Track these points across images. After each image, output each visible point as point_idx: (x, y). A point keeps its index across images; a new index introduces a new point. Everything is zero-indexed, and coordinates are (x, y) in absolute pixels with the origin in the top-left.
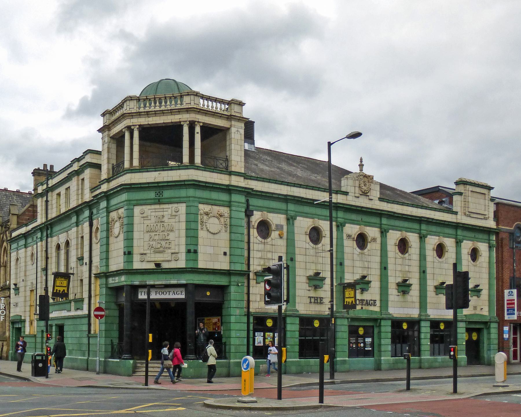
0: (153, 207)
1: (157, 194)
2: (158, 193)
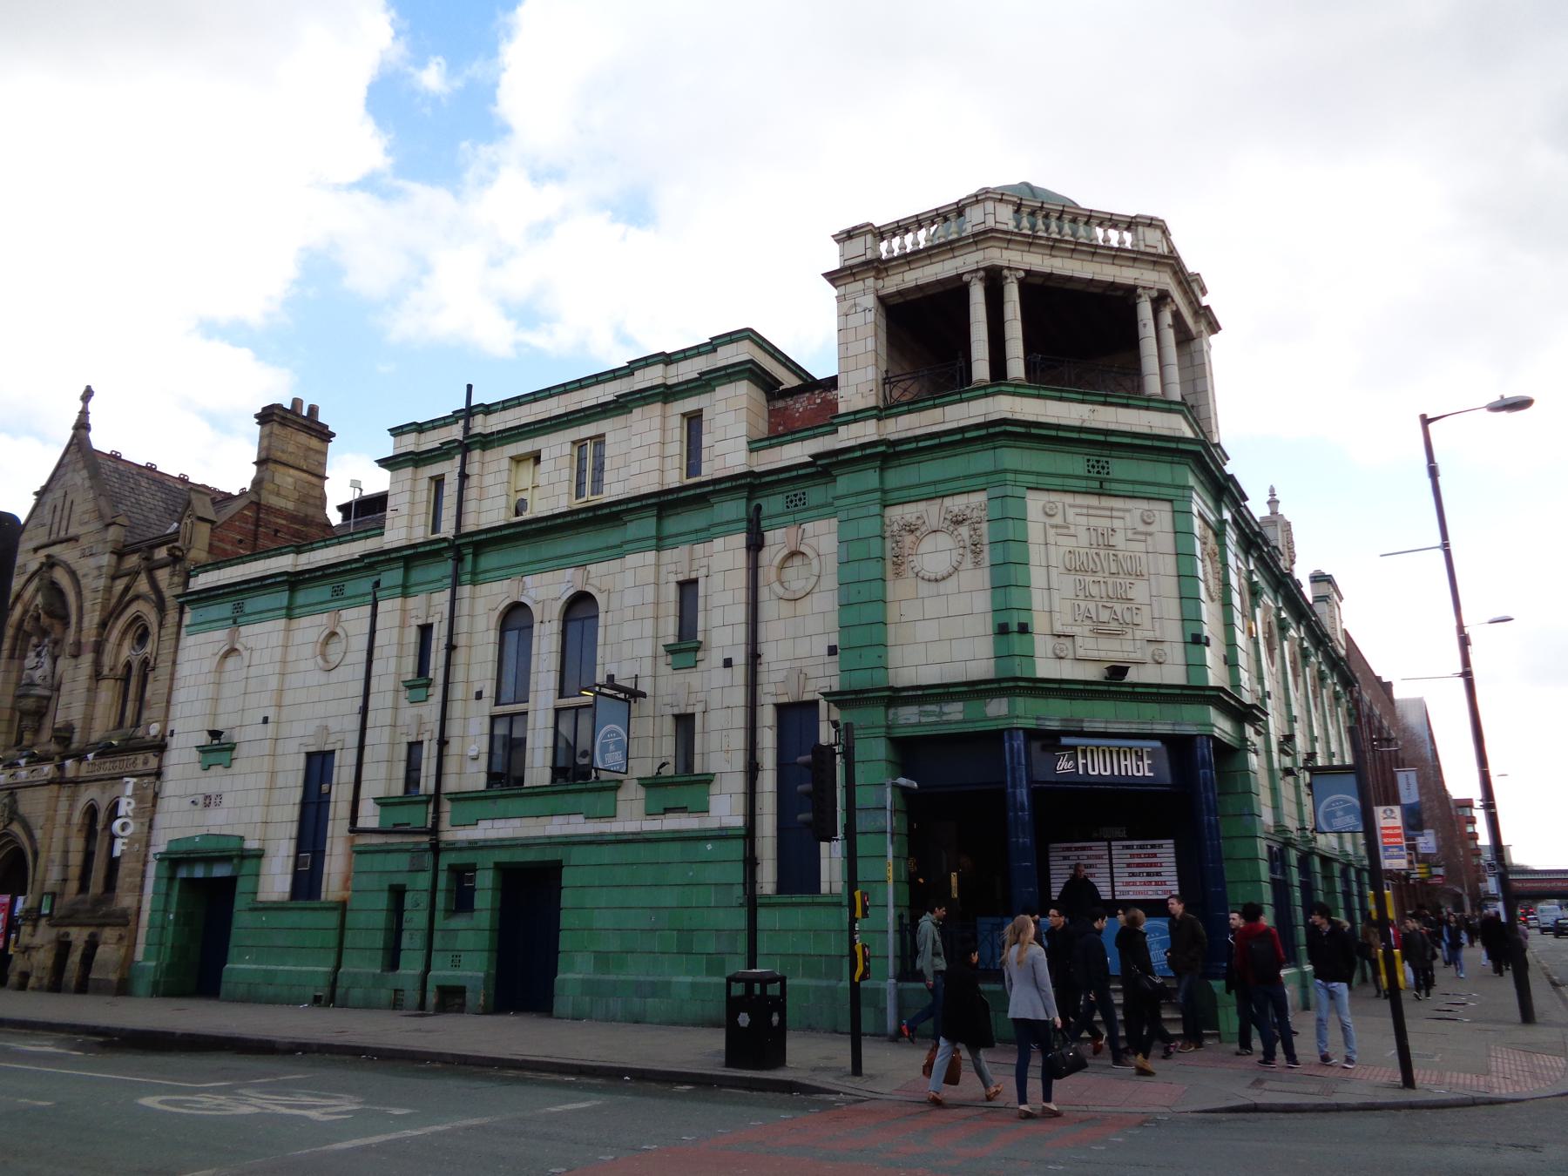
0: (1080, 500)
1: (1093, 467)
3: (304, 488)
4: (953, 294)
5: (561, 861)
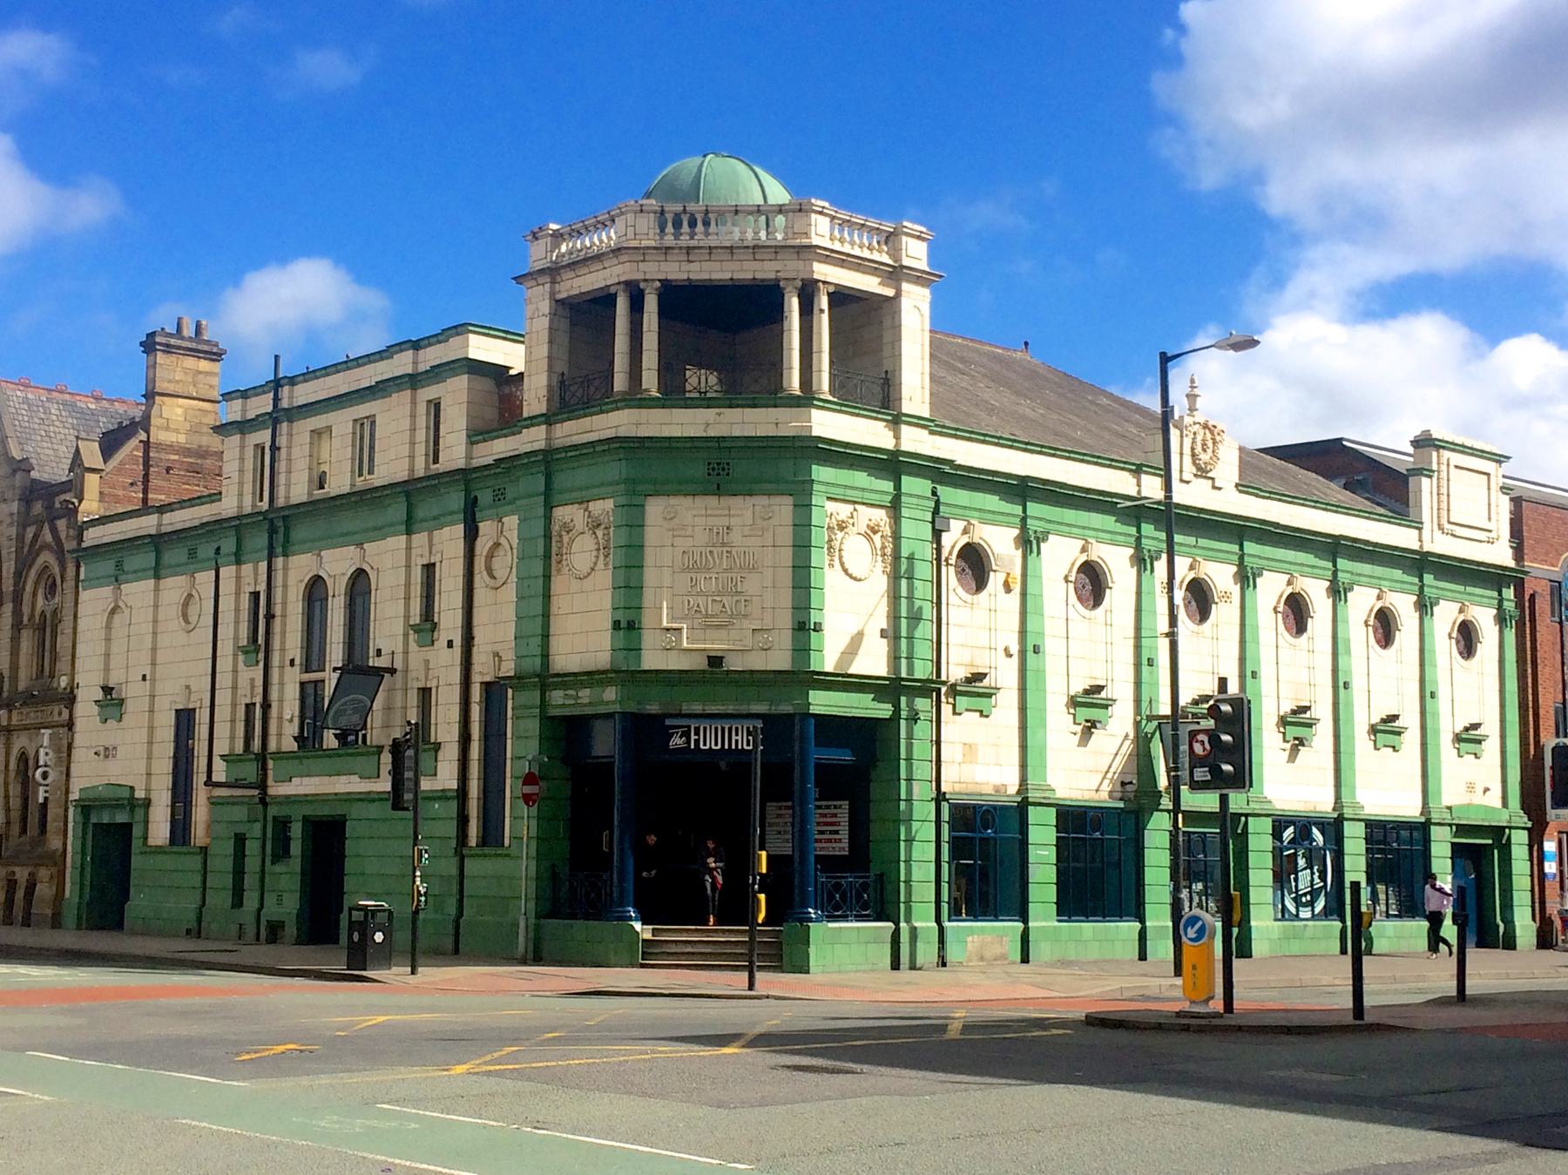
2: (716, 466)
3: (196, 417)
4: (605, 300)
5: (245, 834)
